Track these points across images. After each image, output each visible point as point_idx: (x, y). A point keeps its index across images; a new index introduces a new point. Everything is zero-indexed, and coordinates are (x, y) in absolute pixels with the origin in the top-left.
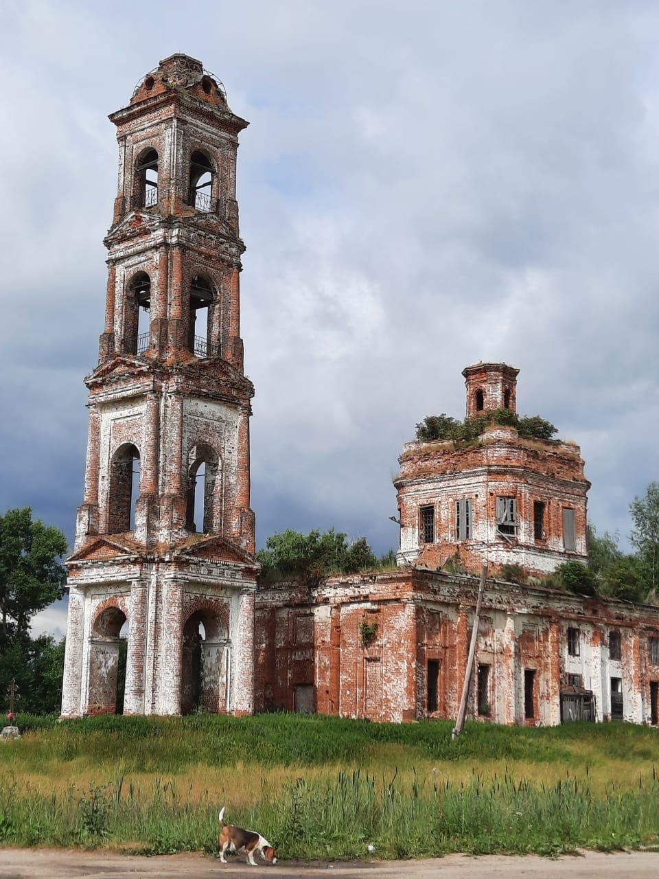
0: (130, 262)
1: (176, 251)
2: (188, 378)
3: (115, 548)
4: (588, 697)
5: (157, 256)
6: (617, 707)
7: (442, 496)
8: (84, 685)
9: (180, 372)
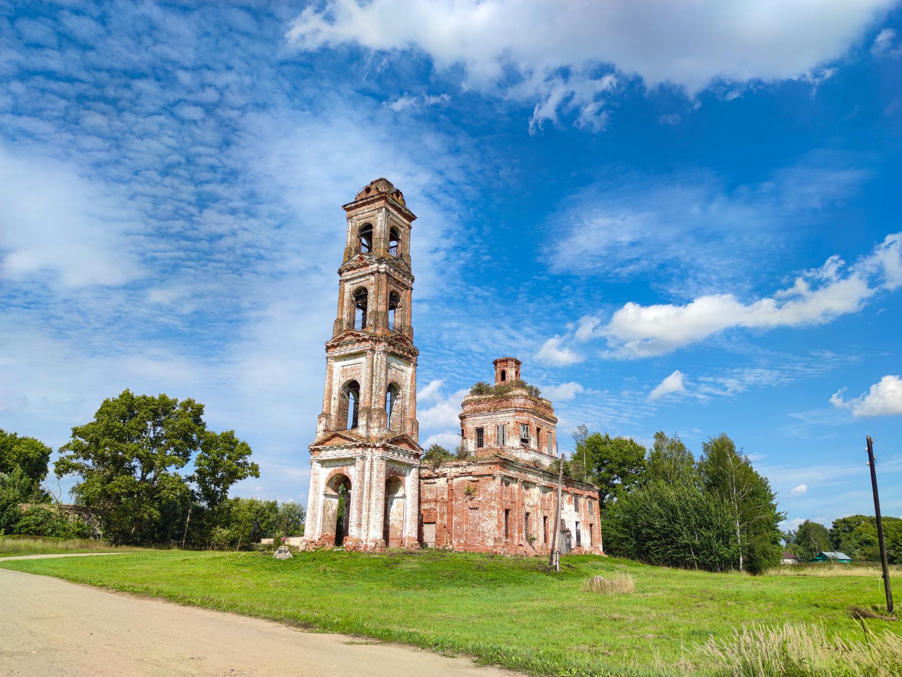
0: (354, 282)
1: (384, 277)
2: (390, 344)
3: (345, 438)
5: (372, 278)
7: (489, 423)
8: (319, 521)
9: (386, 340)
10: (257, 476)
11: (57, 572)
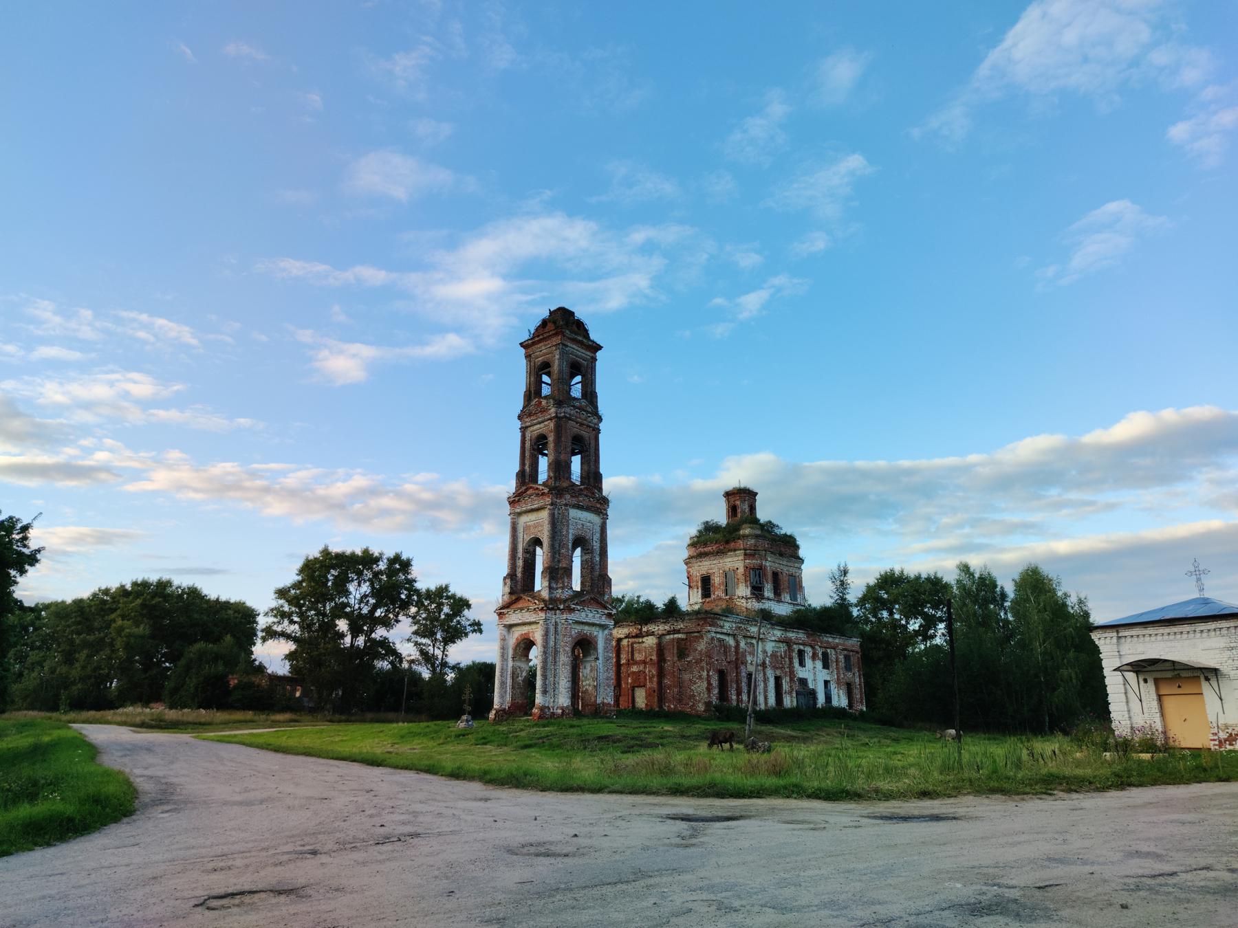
4: (813, 693)
6: (828, 698)
7: (715, 567)
10: (481, 631)
11: (628, 780)
